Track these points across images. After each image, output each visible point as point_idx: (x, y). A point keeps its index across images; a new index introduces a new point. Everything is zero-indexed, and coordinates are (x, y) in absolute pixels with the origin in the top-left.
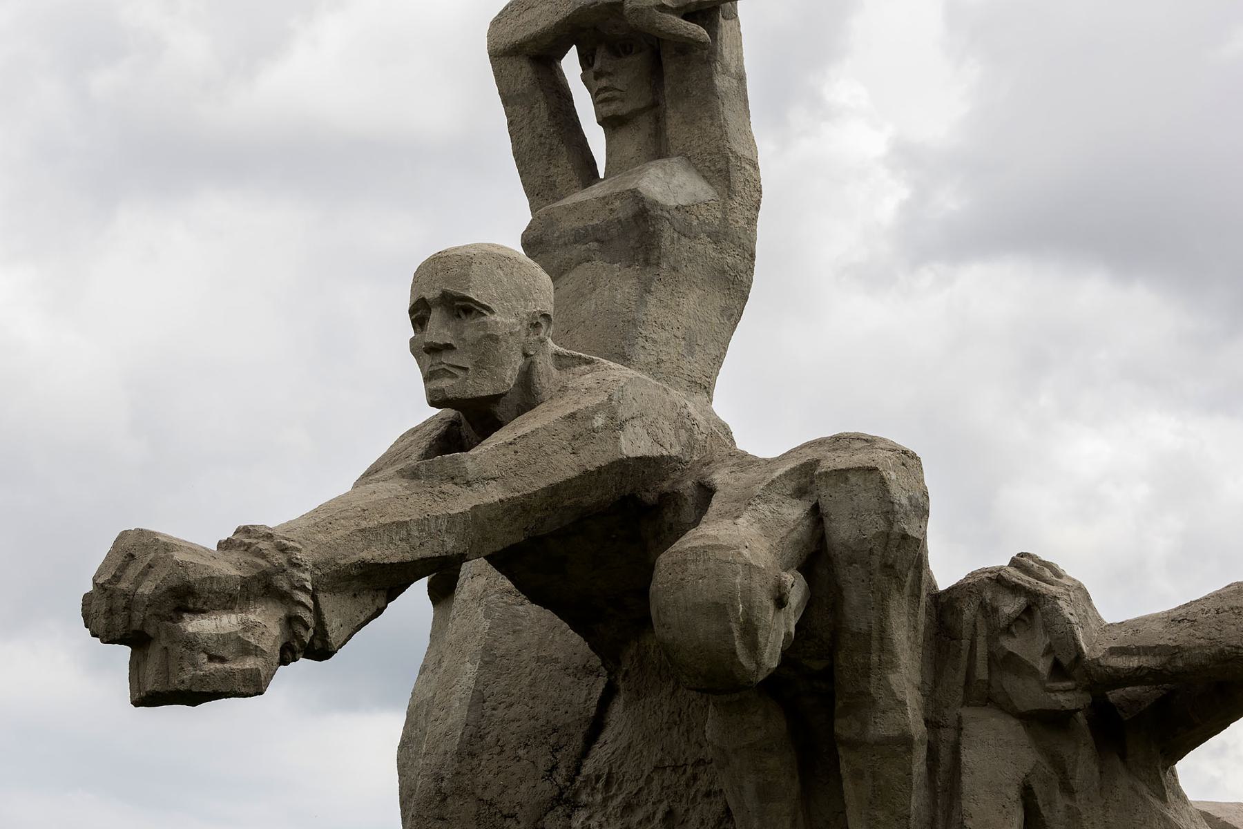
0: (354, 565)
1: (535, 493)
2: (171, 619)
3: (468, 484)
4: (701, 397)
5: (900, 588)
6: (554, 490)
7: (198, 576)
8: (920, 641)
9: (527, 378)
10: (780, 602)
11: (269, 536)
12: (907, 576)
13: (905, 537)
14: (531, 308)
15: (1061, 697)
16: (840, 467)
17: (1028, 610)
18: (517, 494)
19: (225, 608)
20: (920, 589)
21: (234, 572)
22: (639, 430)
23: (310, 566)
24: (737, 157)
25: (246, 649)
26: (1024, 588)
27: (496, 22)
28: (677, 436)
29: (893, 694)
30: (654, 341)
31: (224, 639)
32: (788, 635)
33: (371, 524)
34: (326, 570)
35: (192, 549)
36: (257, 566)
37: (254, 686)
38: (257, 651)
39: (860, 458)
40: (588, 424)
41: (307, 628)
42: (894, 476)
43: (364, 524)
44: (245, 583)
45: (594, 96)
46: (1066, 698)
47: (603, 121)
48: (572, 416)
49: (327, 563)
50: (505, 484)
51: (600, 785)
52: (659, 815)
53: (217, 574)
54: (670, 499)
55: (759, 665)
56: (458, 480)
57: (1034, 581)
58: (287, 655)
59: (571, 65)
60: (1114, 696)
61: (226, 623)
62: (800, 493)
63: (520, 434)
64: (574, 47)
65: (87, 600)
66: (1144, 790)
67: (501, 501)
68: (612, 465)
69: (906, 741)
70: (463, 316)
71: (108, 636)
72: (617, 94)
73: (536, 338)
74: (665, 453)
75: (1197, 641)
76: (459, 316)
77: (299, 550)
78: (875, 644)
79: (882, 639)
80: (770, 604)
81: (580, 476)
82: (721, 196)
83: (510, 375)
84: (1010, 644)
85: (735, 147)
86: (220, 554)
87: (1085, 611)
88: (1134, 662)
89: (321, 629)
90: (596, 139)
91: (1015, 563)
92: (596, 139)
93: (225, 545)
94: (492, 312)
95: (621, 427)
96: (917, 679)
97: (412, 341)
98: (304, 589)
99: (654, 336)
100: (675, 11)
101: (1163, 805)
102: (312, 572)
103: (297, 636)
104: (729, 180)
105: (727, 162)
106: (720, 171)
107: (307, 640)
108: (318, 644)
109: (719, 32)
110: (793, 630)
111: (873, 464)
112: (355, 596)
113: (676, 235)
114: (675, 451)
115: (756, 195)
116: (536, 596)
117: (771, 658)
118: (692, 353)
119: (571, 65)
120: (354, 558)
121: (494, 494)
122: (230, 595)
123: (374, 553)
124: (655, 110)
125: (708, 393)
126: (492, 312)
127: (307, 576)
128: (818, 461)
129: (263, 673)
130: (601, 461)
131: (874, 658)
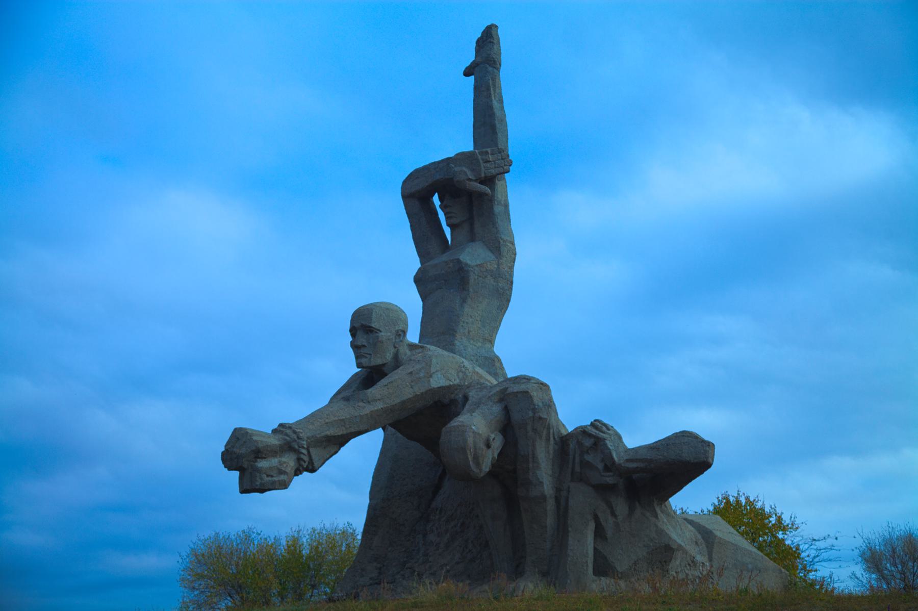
0: (323, 437)
1: (396, 405)
2: (253, 461)
3: (369, 402)
4: (488, 345)
5: (541, 437)
6: (403, 402)
7: (262, 445)
8: (551, 457)
9: (396, 357)
10: (488, 446)
11: (290, 428)
12: (543, 432)
13: (540, 418)
14: (397, 328)
15: (608, 479)
16: (515, 391)
17: (595, 444)
18: (388, 405)
19: (273, 456)
20: (549, 437)
21: (277, 442)
22: (439, 376)
23: (305, 438)
24: (504, 241)
25: (281, 472)
26: (593, 435)
27: (405, 182)
28: (458, 375)
29: (538, 479)
30: (467, 323)
31: (271, 468)
32: (493, 458)
33: (330, 421)
34: (312, 439)
35: (260, 433)
36: (285, 440)
37: (284, 485)
38: (285, 473)
39: (523, 387)
40: (417, 376)
41: (305, 462)
42: (535, 394)
43: (327, 421)
44: (281, 446)
45: (445, 215)
46: (610, 479)
47: (448, 225)
48: (411, 373)
49: (313, 437)
50: (383, 401)
51: (438, 512)
52: (459, 525)
53: (269, 444)
54: (453, 402)
55: (481, 470)
56: (365, 401)
57: (597, 432)
58: (298, 472)
59: (436, 199)
60: (635, 476)
61: (274, 462)
62: (501, 400)
63: (390, 381)
64: (436, 194)
65: (223, 454)
66: (648, 514)
67: (382, 408)
68: (426, 392)
69: (544, 498)
70: (370, 333)
71: (230, 468)
72: (453, 215)
73: (399, 340)
74: (451, 383)
75: (659, 457)
76: (368, 333)
77: (301, 433)
78: (531, 460)
79: (533, 457)
80: (484, 448)
81: (414, 397)
82: (497, 258)
83: (389, 356)
84: (589, 458)
85: (503, 237)
86: (272, 435)
87: (618, 444)
88: (634, 465)
89: (311, 461)
90: (447, 231)
91: (592, 424)
92: (447, 231)
93: (275, 431)
94: (381, 331)
95: (431, 376)
96: (550, 472)
97: (351, 342)
98: (303, 447)
99: (467, 321)
100: (476, 181)
101: (657, 521)
102: (307, 441)
103: (300, 465)
104: (500, 251)
105: (500, 244)
106: (497, 247)
107: (305, 467)
108: (310, 467)
109: (496, 187)
110: (496, 456)
111: (527, 390)
112: (325, 448)
113: (476, 277)
114: (457, 382)
115: (513, 256)
116: (410, 437)
117: (486, 466)
118: (484, 326)
119: (436, 199)
120: (323, 434)
121: (379, 406)
122: (275, 451)
123: (331, 432)
124: (471, 220)
125: (491, 343)
126: (381, 331)
127: (305, 442)
128: (508, 388)
129: (287, 481)
130: (423, 390)
131: (531, 465)
